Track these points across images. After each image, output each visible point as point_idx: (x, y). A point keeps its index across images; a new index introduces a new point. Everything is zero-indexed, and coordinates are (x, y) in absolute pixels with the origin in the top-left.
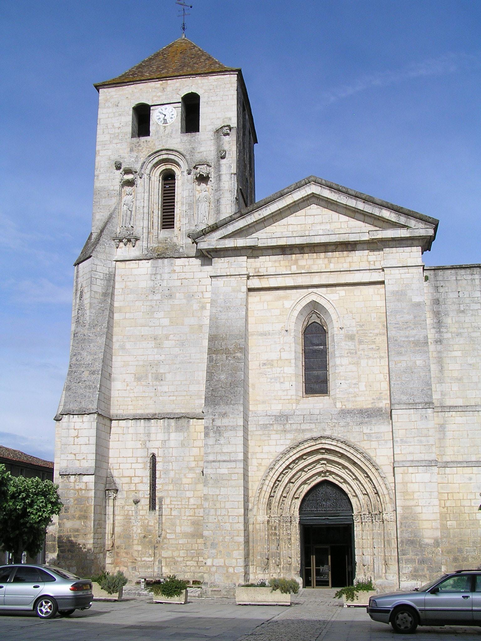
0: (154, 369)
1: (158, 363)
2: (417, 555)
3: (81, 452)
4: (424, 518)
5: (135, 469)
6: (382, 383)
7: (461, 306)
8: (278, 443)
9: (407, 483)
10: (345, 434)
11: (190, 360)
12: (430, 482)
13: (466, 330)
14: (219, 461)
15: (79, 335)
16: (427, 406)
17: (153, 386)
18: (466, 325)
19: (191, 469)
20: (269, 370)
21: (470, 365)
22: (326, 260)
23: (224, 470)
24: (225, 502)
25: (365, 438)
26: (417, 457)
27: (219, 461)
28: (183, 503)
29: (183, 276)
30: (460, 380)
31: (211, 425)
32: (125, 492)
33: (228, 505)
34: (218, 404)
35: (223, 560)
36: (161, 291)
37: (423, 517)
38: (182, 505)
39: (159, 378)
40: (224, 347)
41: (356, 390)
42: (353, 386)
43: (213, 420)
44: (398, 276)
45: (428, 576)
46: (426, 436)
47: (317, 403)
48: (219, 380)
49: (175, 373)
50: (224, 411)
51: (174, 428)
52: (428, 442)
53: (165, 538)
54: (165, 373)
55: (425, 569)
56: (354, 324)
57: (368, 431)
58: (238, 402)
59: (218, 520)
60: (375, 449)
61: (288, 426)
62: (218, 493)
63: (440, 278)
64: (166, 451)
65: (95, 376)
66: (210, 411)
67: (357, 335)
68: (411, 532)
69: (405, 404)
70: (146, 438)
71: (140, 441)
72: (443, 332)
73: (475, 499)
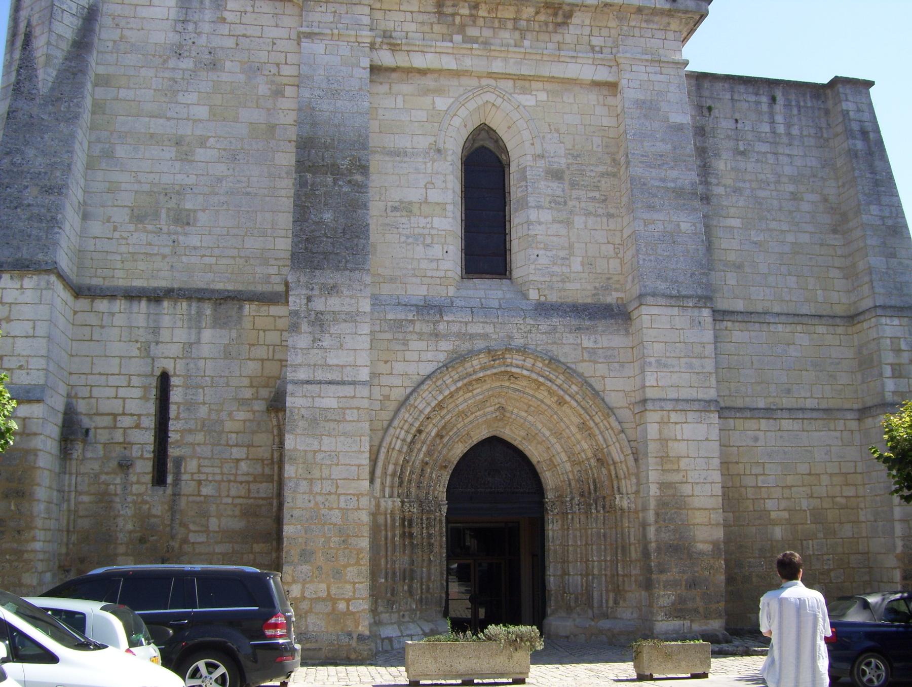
0: (174, 200)
1: (181, 192)
2: (684, 572)
3: (16, 353)
4: (697, 505)
5: (124, 399)
6: (611, 261)
7: (741, 143)
8: (423, 358)
9: (667, 440)
10: (549, 347)
11: (249, 190)
12: (707, 439)
13: (747, 185)
14: (320, 383)
15: (20, 114)
16: (701, 304)
17: (169, 234)
18: (747, 177)
19: (243, 402)
20: (405, 220)
21: (756, 243)
22: (517, 34)
23: (329, 400)
24: (331, 465)
25: (586, 356)
26: (685, 393)
28: (225, 470)
29: (240, 30)
30: (739, 267)
31: (304, 308)
32: (100, 447)
33: (336, 472)
34: (319, 267)
35: (323, 586)
36: (194, 54)
37: (696, 502)
38: (222, 474)
39: (183, 219)
41: (565, 269)
42: (559, 262)
43: (309, 299)
44: (645, 77)
45: (701, 610)
47: (487, 290)
48: (320, 223)
49: (218, 211)
50: (331, 282)
51: (209, 320)
53: (185, 541)
54: (195, 211)
55: (698, 599)
56: (562, 152)
59: (317, 504)
60: (603, 378)
61: (442, 327)
62: (316, 446)
63: (706, 93)
64: (192, 365)
65: (52, 197)
66: (303, 279)
67: (567, 172)
69: (664, 295)
70: (150, 337)
71: (137, 342)
72: (711, 183)
73: (764, 474)
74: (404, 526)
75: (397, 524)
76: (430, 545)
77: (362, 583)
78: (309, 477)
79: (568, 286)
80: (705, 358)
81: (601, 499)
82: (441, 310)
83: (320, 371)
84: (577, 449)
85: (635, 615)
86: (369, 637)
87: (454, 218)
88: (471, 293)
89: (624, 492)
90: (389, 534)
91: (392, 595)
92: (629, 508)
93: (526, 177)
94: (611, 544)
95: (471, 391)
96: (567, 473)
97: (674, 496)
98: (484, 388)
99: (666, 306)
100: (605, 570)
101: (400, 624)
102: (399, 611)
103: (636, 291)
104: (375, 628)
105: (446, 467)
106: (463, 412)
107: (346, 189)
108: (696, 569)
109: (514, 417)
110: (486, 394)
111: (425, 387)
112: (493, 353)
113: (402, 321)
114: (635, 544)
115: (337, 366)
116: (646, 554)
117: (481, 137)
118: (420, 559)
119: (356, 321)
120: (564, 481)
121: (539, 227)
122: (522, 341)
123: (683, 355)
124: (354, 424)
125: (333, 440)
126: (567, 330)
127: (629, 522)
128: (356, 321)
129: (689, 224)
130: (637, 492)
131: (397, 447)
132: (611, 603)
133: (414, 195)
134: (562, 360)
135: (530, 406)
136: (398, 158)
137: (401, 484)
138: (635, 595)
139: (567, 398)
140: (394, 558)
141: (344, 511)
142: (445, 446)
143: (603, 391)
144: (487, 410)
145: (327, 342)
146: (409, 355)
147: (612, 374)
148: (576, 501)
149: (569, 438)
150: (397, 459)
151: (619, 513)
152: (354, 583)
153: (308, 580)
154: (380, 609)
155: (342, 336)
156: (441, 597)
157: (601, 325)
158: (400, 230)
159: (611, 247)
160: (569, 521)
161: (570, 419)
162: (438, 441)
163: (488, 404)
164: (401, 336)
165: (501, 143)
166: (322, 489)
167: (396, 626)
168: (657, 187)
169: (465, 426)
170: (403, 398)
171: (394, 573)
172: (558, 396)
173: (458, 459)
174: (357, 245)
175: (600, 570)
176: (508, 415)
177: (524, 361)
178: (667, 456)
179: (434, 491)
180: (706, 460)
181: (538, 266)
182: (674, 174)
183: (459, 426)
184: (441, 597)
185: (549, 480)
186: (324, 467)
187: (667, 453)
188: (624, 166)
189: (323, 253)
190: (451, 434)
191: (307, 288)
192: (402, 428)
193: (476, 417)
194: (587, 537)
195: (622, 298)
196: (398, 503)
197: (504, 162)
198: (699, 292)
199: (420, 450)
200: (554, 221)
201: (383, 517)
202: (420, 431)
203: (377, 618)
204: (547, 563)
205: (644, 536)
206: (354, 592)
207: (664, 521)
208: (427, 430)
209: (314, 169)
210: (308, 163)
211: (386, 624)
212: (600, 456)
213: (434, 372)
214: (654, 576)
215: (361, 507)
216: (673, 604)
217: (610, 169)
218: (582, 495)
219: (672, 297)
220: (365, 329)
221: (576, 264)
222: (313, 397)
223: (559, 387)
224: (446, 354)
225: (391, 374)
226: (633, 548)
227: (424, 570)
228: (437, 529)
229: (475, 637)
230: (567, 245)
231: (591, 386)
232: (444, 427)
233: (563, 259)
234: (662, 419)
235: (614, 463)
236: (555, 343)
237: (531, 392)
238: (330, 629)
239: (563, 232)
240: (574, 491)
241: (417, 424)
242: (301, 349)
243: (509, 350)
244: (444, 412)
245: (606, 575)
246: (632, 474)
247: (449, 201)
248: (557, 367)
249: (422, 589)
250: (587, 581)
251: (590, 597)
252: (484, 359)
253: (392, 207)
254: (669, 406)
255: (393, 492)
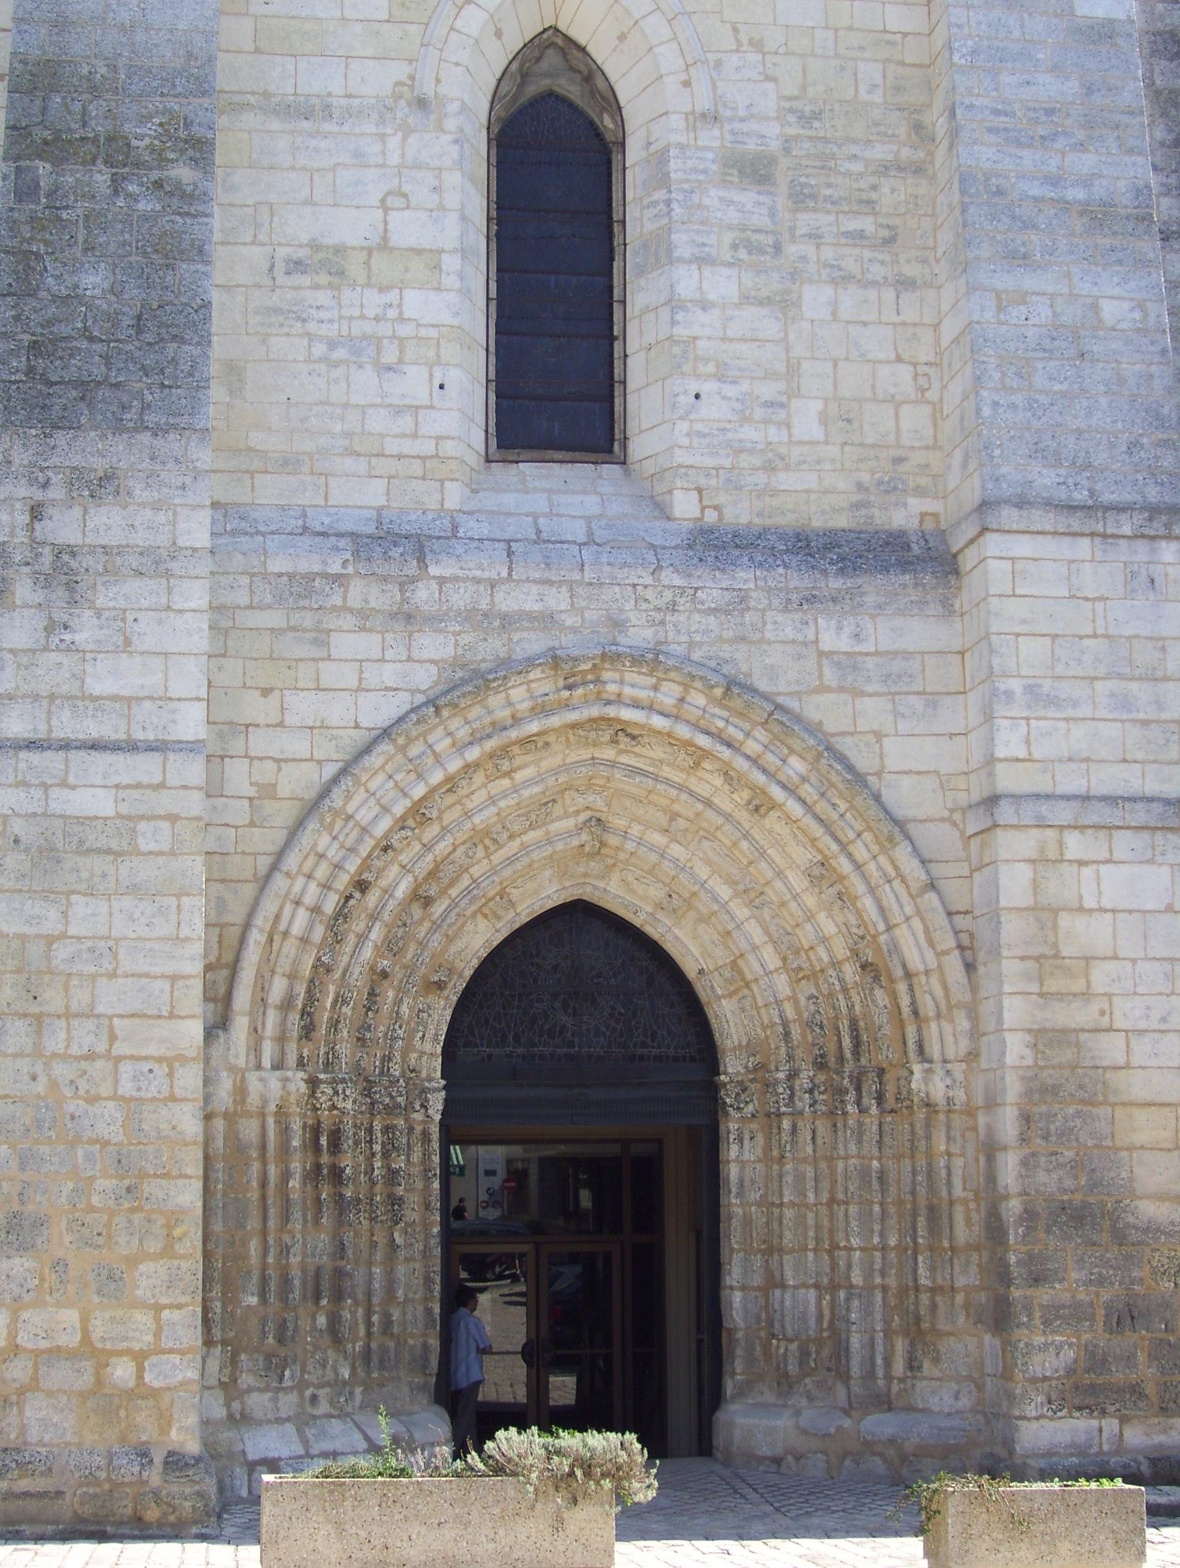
2: (1101, 1281)
6: (905, 410)
8: (371, 680)
9: (1055, 911)
10: (726, 651)
14: (65, 746)
16: (1157, 527)
20: (323, 297)
24: (94, 977)
26: (1129, 780)
27: (65, 746)
31: (21, 537)
33: (111, 998)
35: (71, 1317)
37: (1137, 1086)
40: (99, 127)
42: (759, 413)
43: (36, 512)
45: (1150, 1389)
46: (1154, 677)
47: (557, 493)
50: (100, 465)
52: (1160, 705)
55: (1141, 1357)
56: (770, 105)
57: (844, 644)
58: (184, 421)
59: (54, 1085)
60: (879, 736)
61: (423, 595)
62: (52, 923)
67: (784, 162)
68: (1075, 1166)
69: (1050, 504)
74: (317, 1149)
75: (296, 1143)
76: (395, 1202)
77: (179, 1307)
78: (34, 1009)
79: (785, 480)
80: (1166, 679)
81: (872, 1075)
82: (421, 548)
83: (66, 713)
84: (806, 935)
85: (965, 1402)
86: (198, 1460)
87: (465, 292)
88: (509, 500)
89: (936, 1055)
90: (273, 1171)
91: (281, 1340)
92: (949, 1100)
93: (668, 174)
94: (900, 1203)
95: (508, 774)
96: (778, 1003)
97: (1074, 1068)
98: (545, 765)
99: (1055, 533)
100: (883, 1274)
101: (302, 1421)
102: (301, 1386)
103: (972, 492)
104: (227, 1435)
105: (440, 986)
106: (487, 833)
107: (144, 206)
108: (1136, 1274)
109: (630, 846)
110: (551, 782)
111: (374, 761)
112: (567, 668)
113: (310, 577)
114: (965, 1202)
115: (115, 698)
116: (995, 1230)
117: (544, 65)
118: (363, 1243)
119: (168, 575)
120: (772, 1025)
121: (701, 316)
122: (649, 633)
123: (1102, 670)
124: (161, 860)
125: (103, 907)
126: (776, 602)
127: (949, 1139)
128: (168, 575)
129: (1126, 305)
130: (972, 1056)
131: (297, 929)
132: (899, 1367)
133: (350, 227)
134: (763, 685)
135: (674, 816)
136: (306, 125)
137: (308, 1031)
138: (965, 1345)
139: (777, 793)
140: (287, 1238)
141: (132, 1105)
142: (436, 926)
143: (879, 774)
144: (555, 827)
145: (86, 631)
146: (330, 673)
147: (903, 726)
148: (803, 1080)
149: (783, 904)
150: (297, 961)
151: (921, 1114)
152: (158, 1308)
153: (27, 1298)
154: (246, 1379)
155: (130, 617)
156: (425, 1346)
157: (873, 587)
158: (312, 326)
159: (905, 373)
160: (785, 1137)
161: (787, 849)
162: (417, 911)
163: (558, 810)
164: (308, 620)
165: (600, 83)
166: (69, 1040)
167: (290, 1428)
168: (1036, 199)
169: (494, 871)
170: (311, 794)
171: (286, 1281)
172: (752, 787)
173: (475, 963)
174: (174, 361)
175: (868, 1273)
176: (613, 840)
177: (655, 688)
178: (1056, 956)
179: (405, 1055)
180: (1167, 966)
181: (699, 427)
182: (1087, 162)
183: (476, 871)
184: (425, 1346)
185: (731, 1022)
186: (75, 981)
187: (1055, 945)
188: (946, 143)
189: (79, 383)
190: (454, 892)
191: (33, 481)
192: (309, 877)
193: (524, 846)
194: (834, 1182)
195: (935, 515)
196: (298, 1083)
197: (610, 137)
198: (1153, 494)
199: (362, 937)
200: (746, 299)
201: (254, 1124)
202: (362, 886)
203: (236, 1405)
204: (724, 1257)
205: (991, 1178)
206: (158, 1334)
207: (1046, 1137)
208: (383, 883)
209: (58, 149)
210: (39, 134)
211: (260, 1423)
212: (869, 955)
213: (401, 720)
214: (1016, 1293)
215: (178, 1092)
216: (1070, 1372)
217: (906, 153)
218: (820, 1064)
219: (1073, 508)
220: (195, 595)
221: (807, 421)
222: (46, 787)
223: (754, 761)
224: (434, 670)
225: (281, 724)
226: (959, 1213)
227: (377, 1270)
228: (416, 1157)
229: (459, 1464)
230: (781, 368)
231: (842, 759)
232: (432, 875)
233: (769, 404)
234: (1042, 850)
235: (908, 975)
236: (743, 639)
237: (678, 777)
238: (90, 1438)
239: (770, 327)
240: (799, 1053)
241: (352, 865)
242: (12, 651)
243: (610, 658)
244: (433, 830)
245: (885, 1289)
246: (959, 1006)
247: (450, 244)
248: (748, 705)
249: (369, 1324)
250: (833, 1305)
251: (841, 1350)
252: (543, 683)
253: (288, 261)
254: (1063, 814)
255: (283, 1053)
